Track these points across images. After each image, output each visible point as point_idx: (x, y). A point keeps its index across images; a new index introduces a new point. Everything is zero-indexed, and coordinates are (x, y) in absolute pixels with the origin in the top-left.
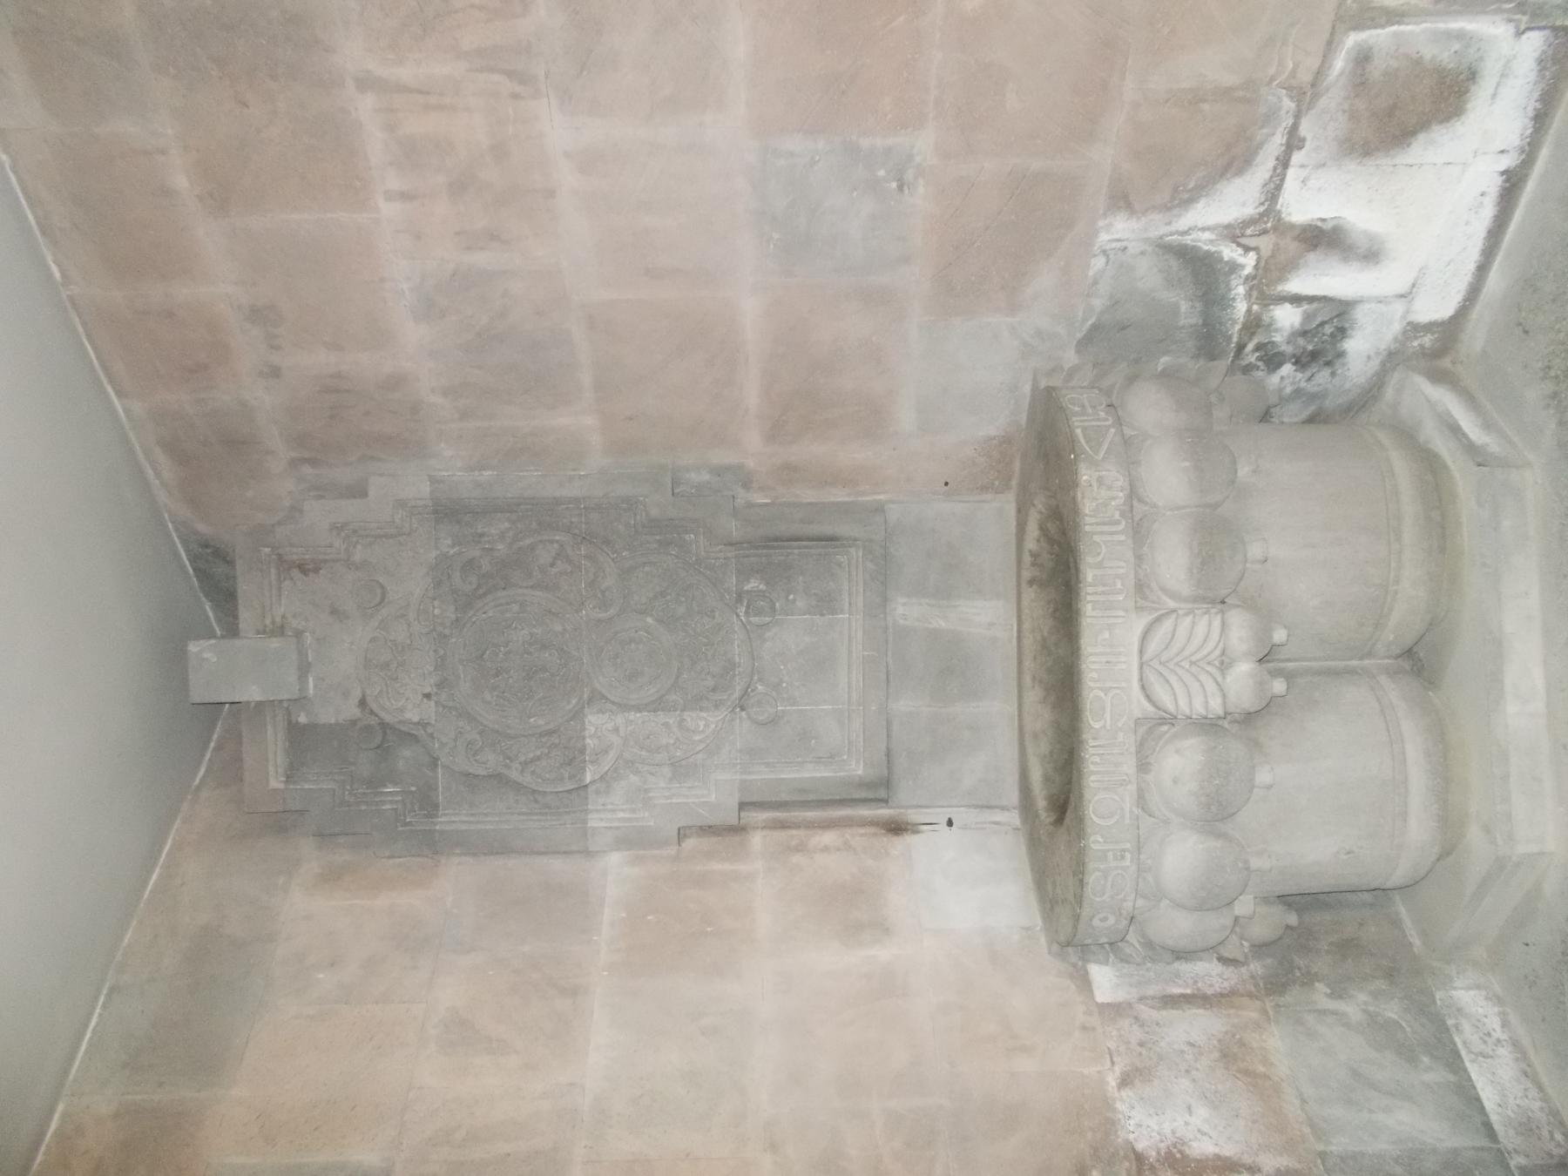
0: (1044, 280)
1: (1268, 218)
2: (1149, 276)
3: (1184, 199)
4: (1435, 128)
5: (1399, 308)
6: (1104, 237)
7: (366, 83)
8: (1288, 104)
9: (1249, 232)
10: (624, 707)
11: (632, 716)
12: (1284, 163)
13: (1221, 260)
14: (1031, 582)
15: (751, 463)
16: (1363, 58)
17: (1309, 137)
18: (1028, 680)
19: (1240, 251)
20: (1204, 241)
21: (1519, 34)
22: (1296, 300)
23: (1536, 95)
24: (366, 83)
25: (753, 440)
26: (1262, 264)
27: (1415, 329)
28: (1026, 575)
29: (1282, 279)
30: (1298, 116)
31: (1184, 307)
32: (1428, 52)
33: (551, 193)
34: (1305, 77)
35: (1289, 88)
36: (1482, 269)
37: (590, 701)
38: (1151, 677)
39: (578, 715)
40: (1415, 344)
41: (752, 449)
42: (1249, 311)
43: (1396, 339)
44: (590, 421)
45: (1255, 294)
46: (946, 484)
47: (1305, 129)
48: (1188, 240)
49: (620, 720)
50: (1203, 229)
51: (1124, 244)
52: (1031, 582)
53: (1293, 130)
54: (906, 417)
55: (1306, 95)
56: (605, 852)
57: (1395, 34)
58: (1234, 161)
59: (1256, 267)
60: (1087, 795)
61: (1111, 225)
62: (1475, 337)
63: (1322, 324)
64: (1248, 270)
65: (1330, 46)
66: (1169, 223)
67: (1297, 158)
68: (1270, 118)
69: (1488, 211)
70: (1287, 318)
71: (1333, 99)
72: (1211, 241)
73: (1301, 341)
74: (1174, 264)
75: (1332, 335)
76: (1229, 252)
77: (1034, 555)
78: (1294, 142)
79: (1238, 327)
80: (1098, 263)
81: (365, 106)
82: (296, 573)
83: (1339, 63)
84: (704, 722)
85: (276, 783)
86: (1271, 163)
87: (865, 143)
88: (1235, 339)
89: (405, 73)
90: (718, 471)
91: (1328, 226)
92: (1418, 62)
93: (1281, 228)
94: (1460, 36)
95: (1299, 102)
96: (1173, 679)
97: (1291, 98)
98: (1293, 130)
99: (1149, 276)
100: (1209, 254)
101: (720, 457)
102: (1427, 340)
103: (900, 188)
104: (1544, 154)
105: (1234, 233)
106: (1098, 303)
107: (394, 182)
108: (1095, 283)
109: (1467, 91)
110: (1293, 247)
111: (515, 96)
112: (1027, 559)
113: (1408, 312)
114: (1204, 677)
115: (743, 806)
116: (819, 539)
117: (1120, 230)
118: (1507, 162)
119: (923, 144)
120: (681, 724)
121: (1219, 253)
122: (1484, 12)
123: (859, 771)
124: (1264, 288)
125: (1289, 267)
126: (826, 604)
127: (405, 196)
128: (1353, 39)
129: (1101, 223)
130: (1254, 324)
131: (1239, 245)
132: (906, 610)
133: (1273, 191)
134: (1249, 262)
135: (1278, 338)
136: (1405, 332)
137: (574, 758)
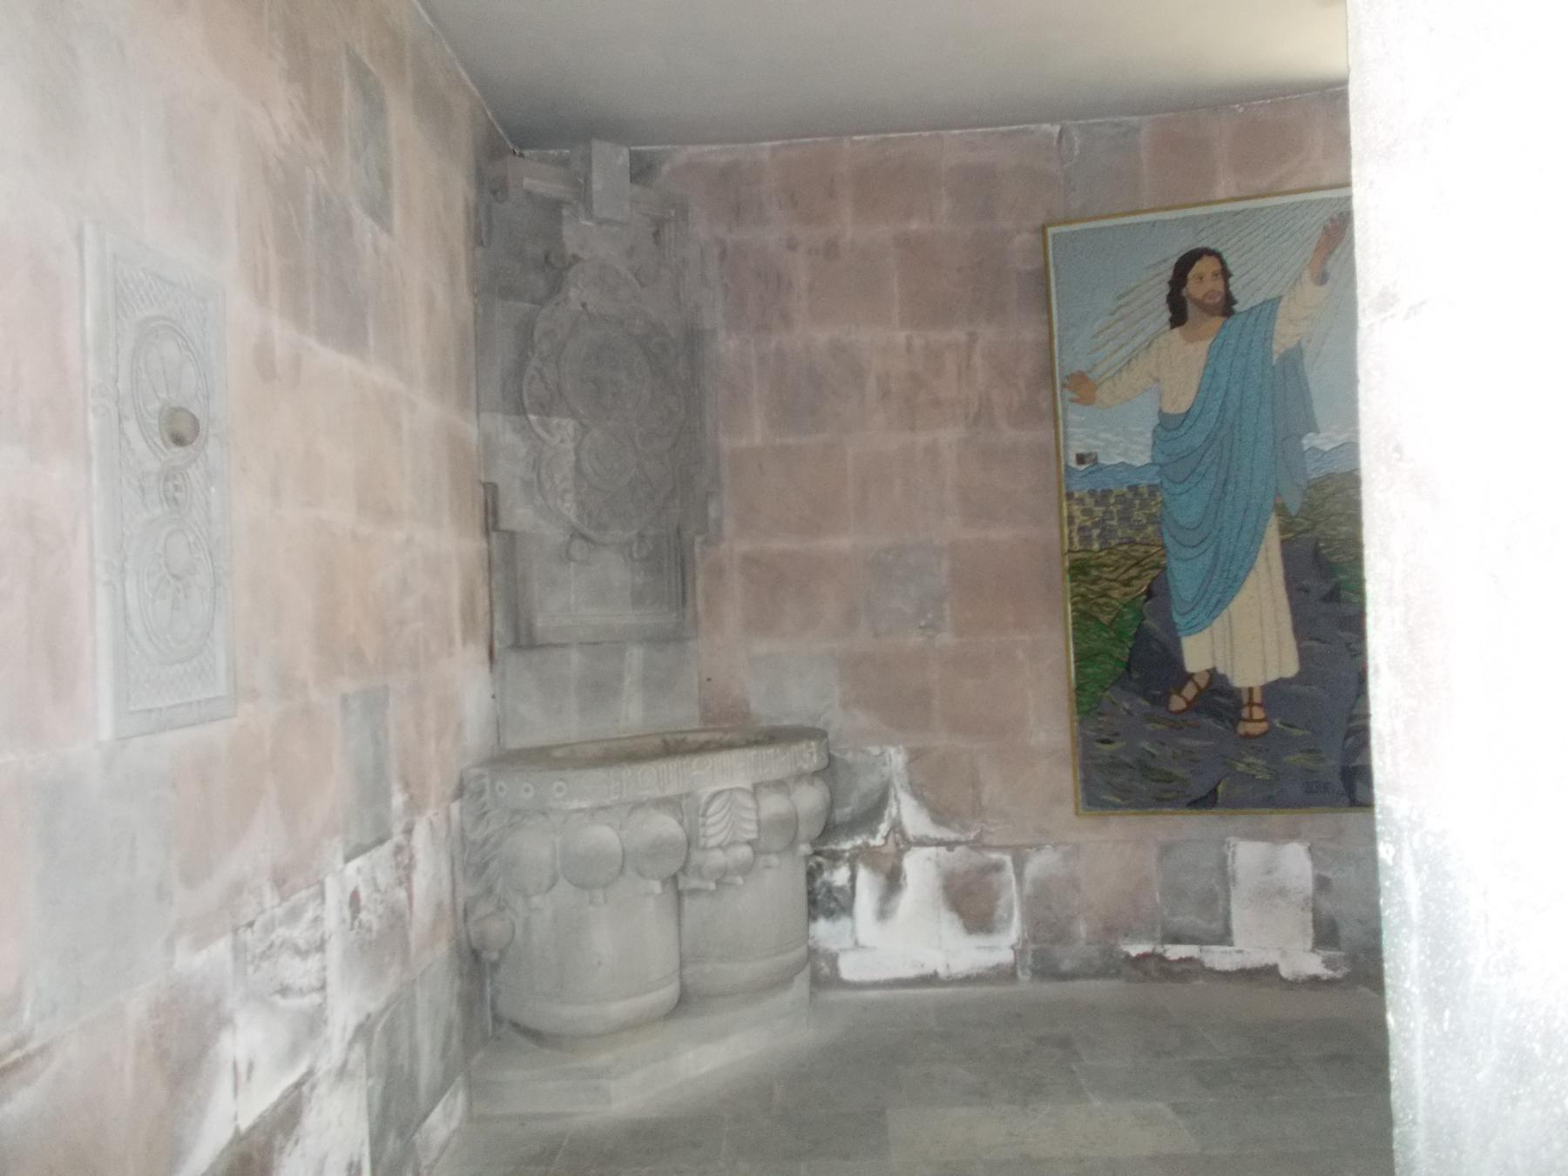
0: (863, 719)
1: (904, 842)
2: (868, 783)
3: (917, 793)
4: (961, 921)
5: (848, 943)
6: (892, 750)
7: (973, 337)
8: (972, 835)
9: (897, 835)
10: (577, 450)
11: (572, 457)
12: (939, 843)
13: (879, 823)
14: (665, 741)
15: (724, 546)
16: (998, 867)
17: (955, 853)
18: (606, 745)
19: (885, 834)
20: (891, 810)
21: (1012, 947)
22: (853, 878)
23: (980, 971)
24: (973, 337)
25: (744, 546)
26: (877, 850)
27: (833, 959)
28: (669, 738)
29: (867, 865)
30: (966, 843)
31: (848, 810)
32: (1002, 902)
33: (913, 429)
34: (986, 840)
35: (980, 834)
36: (875, 985)
37: (581, 424)
38: (724, 797)
39: (573, 414)
40: (823, 964)
41: (736, 545)
42: (844, 851)
43: (826, 950)
44: (758, 440)
45: (857, 851)
46: (709, 680)
47: (959, 850)
48: (892, 801)
49: (570, 445)
50: (899, 809)
51: (888, 763)
52: (665, 741)
53: (957, 843)
54: (762, 647)
55: (977, 845)
56: (479, 426)
57: (1011, 881)
58: (939, 815)
59: (874, 847)
60: (655, 763)
61: (899, 753)
62: (833, 996)
63: (836, 900)
64: (872, 842)
65: (1001, 848)
66: (902, 787)
67: (942, 850)
68: (965, 828)
69: (910, 972)
70: (840, 876)
71: (977, 859)
72: (890, 815)
73: (824, 890)
74: (876, 796)
75: (829, 909)
76: (884, 828)
77: (683, 740)
78: (950, 845)
79: (833, 847)
80: (875, 751)
81: (958, 335)
82: (652, 229)
83: (995, 856)
84: (569, 508)
85: (527, 182)
86: (939, 836)
87: (946, 605)
88: (825, 848)
89: (977, 360)
90: (719, 523)
91: (902, 882)
92: (997, 898)
93: (900, 854)
94: (1011, 916)
95: (973, 841)
96: (724, 812)
97: (976, 836)
98: (957, 843)
99: (868, 783)
100: (882, 815)
101: (729, 525)
102: (826, 970)
103: (921, 627)
104: (949, 990)
105: (897, 827)
106: (849, 757)
107: (918, 342)
108: (863, 752)
109: (982, 931)
110: (888, 865)
111: (966, 417)
112: (680, 737)
113: (845, 950)
114: (725, 832)
115: (512, 535)
116: (684, 593)
117: (897, 758)
118: (942, 972)
119: (946, 638)
120: (565, 491)
121: (883, 821)
122: (1022, 922)
123: (539, 622)
124: (867, 856)
125: (874, 866)
126: (638, 598)
127: (909, 348)
128: (1007, 859)
129: (901, 747)
130: (835, 857)
131: (889, 832)
132: (635, 655)
133: (922, 842)
134: (878, 841)
135: (826, 875)
136: (831, 954)
137: (545, 409)
